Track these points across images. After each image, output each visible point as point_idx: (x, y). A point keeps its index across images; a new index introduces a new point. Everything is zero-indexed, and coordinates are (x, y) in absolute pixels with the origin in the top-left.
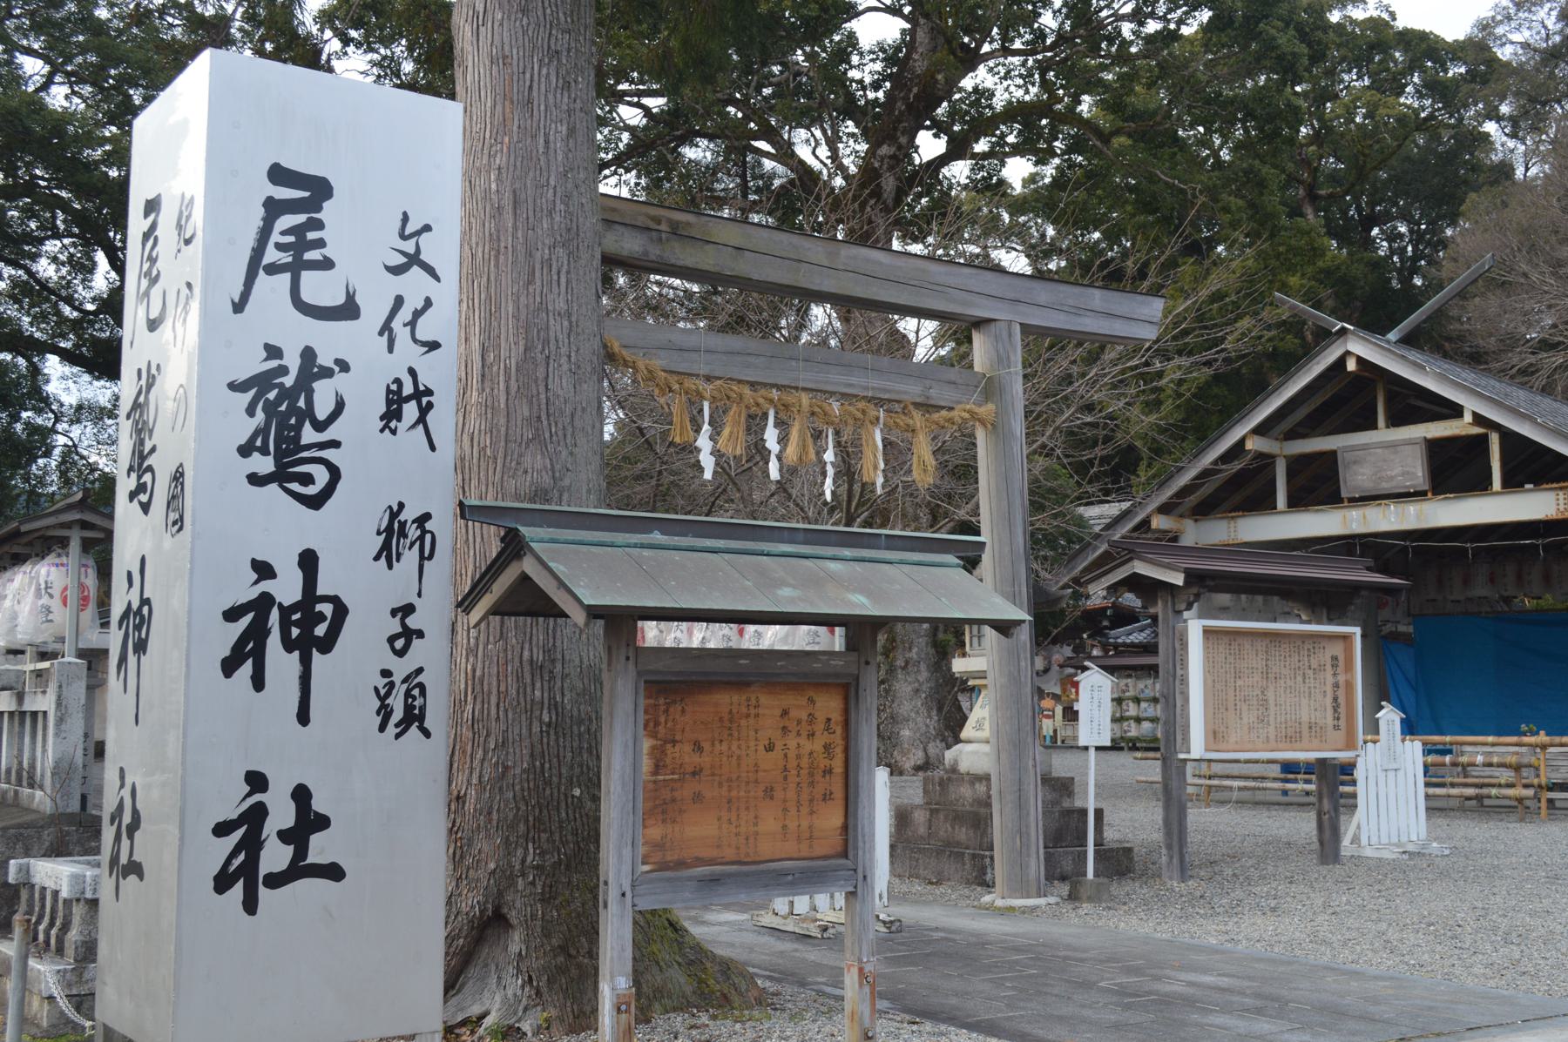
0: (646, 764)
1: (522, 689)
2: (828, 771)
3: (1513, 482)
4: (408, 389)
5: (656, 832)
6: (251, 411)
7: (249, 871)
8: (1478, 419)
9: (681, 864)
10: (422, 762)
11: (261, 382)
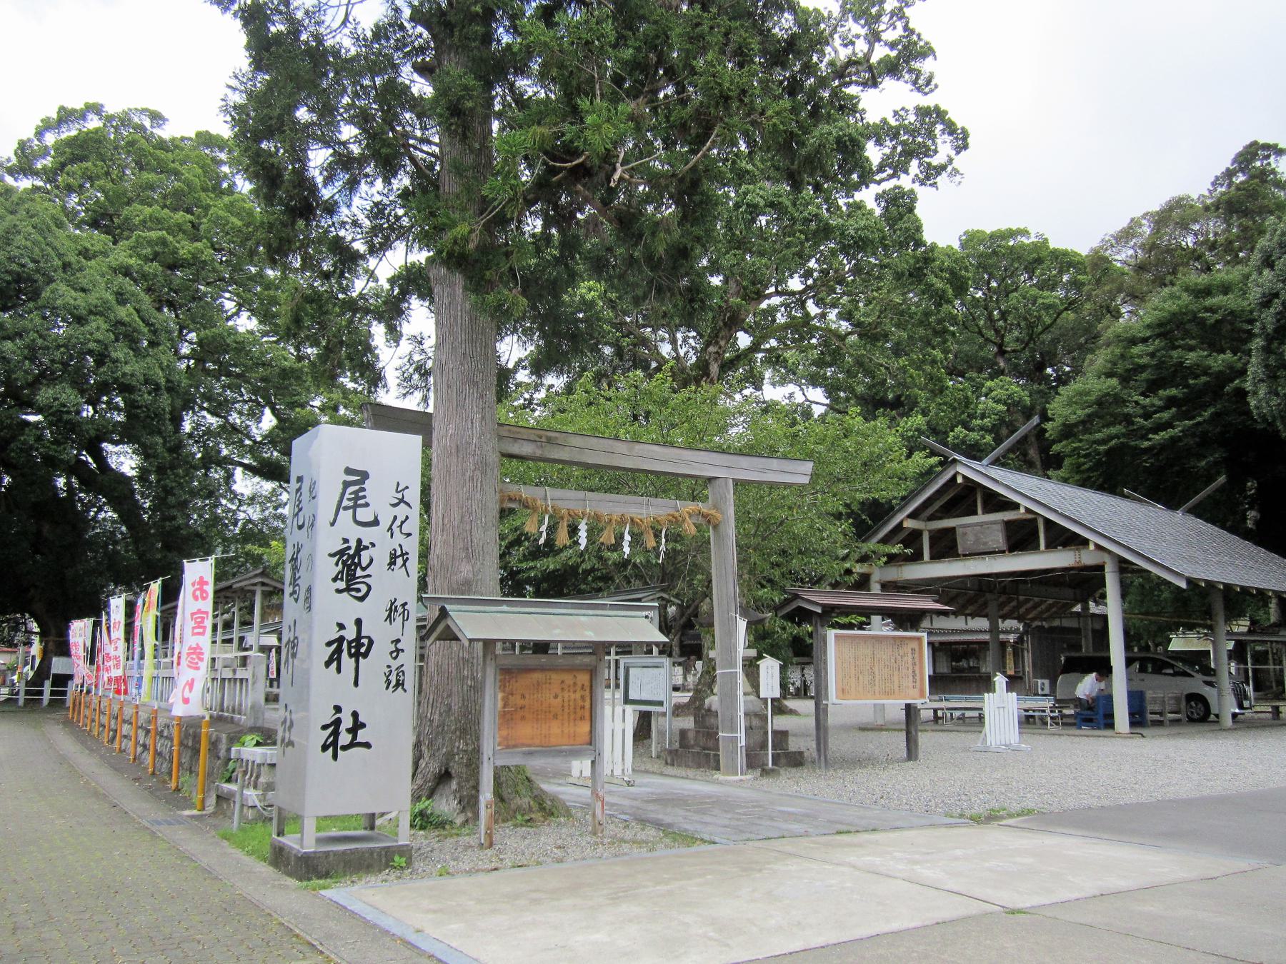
0: (500, 704)
1: (459, 671)
2: (583, 707)
3: (1051, 545)
4: (399, 553)
5: (504, 733)
6: (337, 564)
7: (335, 743)
8: (1028, 511)
9: (515, 746)
10: (405, 701)
11: (341, 553)
